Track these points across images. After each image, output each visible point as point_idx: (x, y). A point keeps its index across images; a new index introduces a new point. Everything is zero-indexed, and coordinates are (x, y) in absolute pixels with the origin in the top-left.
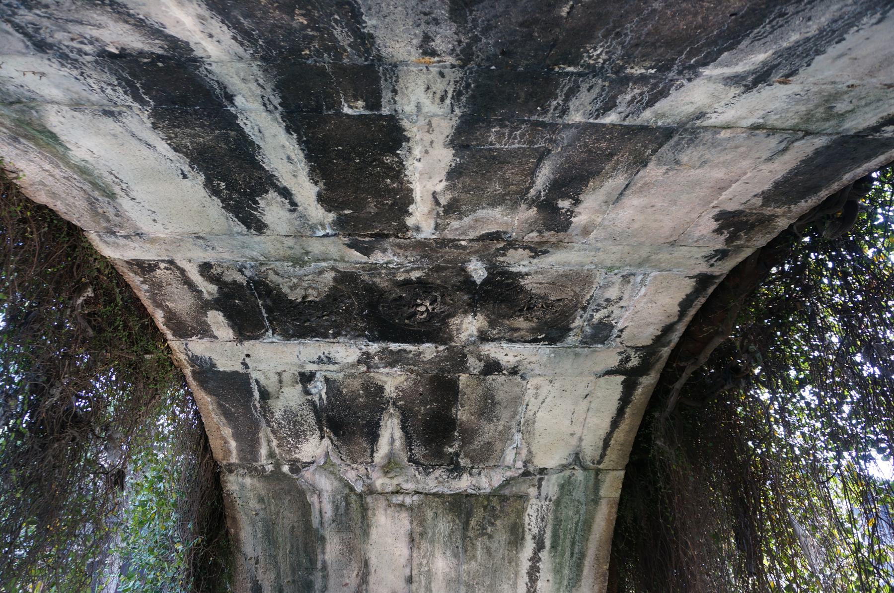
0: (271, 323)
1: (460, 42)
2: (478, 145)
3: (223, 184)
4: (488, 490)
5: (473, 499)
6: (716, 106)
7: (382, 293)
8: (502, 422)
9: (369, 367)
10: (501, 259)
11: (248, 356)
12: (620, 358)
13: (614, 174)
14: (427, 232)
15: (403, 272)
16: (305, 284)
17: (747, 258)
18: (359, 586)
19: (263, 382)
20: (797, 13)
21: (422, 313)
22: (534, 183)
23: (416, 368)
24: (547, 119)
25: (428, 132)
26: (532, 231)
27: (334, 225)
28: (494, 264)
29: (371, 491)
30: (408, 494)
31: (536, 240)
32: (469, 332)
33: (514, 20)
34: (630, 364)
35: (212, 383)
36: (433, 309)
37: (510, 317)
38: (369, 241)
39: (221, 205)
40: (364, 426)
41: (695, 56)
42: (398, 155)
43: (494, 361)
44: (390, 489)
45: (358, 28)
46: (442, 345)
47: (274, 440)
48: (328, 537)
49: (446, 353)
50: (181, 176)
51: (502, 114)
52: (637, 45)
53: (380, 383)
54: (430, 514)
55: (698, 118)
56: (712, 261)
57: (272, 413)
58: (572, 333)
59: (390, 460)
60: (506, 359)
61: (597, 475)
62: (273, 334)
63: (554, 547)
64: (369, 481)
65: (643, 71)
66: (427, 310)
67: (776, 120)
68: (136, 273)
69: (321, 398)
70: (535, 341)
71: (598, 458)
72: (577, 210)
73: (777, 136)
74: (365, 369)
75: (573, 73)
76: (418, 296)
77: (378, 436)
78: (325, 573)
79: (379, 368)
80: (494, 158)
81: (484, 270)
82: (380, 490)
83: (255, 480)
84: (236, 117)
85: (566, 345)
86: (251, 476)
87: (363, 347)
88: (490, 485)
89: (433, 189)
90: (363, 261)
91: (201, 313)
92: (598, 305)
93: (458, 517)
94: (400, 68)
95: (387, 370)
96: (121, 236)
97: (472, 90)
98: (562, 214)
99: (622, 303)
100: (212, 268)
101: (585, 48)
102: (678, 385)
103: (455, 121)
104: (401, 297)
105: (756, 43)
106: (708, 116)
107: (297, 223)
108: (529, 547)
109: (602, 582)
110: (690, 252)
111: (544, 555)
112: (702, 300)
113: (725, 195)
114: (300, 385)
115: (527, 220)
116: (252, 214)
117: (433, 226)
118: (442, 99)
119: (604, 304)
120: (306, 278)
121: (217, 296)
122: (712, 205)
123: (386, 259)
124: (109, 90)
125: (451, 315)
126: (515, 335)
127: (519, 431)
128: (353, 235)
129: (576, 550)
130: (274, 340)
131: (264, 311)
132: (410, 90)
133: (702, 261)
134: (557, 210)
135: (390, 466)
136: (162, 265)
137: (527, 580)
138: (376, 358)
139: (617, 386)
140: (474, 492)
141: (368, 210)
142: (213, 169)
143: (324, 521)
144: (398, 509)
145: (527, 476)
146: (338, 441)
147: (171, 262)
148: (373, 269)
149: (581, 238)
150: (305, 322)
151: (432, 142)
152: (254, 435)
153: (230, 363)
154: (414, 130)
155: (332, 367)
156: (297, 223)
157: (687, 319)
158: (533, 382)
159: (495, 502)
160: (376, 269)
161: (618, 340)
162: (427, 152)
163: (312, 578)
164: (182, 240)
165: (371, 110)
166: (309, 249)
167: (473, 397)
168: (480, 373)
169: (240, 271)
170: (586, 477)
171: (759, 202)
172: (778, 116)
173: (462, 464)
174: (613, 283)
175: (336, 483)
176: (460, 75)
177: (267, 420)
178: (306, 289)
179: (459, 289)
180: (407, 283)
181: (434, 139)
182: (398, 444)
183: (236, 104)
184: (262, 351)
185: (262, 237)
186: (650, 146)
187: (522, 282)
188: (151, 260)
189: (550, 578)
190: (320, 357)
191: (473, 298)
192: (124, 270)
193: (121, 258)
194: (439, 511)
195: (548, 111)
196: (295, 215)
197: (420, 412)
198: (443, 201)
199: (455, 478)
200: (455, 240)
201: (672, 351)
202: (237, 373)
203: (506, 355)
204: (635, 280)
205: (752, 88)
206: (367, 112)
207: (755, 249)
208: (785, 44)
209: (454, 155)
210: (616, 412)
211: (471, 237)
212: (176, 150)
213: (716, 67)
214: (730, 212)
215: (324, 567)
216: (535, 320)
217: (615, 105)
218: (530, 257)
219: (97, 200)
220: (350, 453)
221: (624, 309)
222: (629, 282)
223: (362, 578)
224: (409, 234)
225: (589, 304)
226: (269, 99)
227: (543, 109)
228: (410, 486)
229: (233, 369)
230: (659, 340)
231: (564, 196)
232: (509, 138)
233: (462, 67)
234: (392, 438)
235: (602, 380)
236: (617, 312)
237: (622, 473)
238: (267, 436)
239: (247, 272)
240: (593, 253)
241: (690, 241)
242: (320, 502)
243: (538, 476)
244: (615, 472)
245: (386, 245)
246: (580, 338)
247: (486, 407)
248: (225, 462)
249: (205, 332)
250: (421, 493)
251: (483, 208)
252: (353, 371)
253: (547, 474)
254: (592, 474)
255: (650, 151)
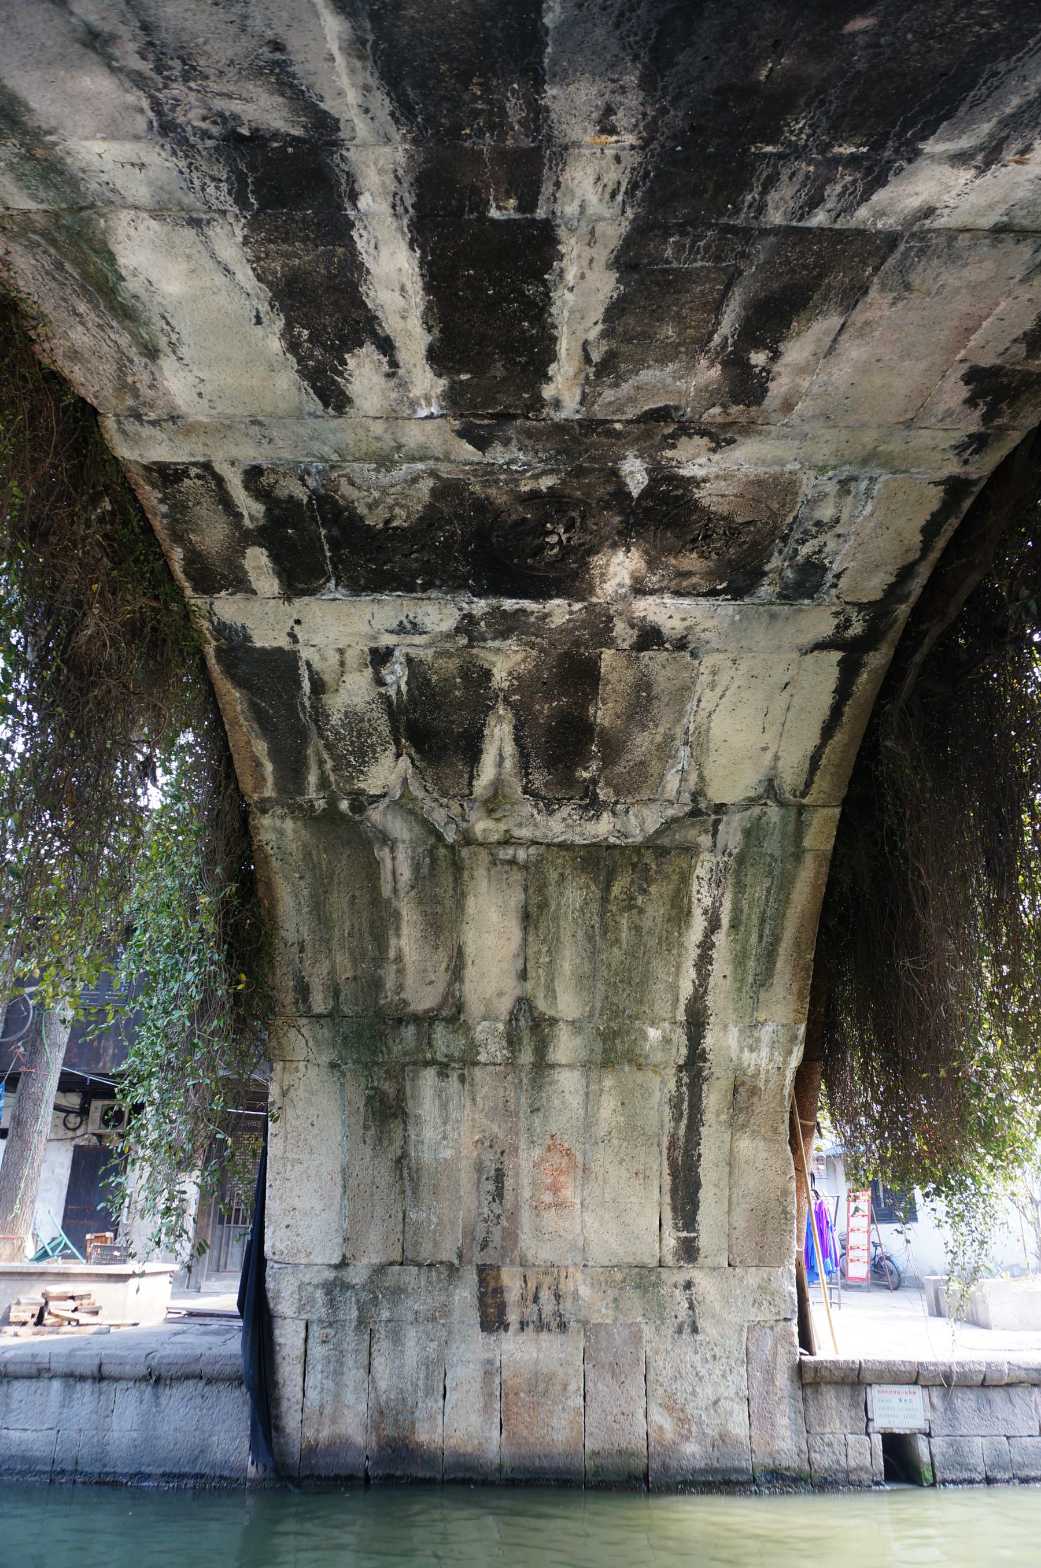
0: (335, 568)
1: (645, 115)
2: (650, 263)
3: (306, 332)
4: (639, 839)
5: (617, 852)
6: (946, 197)
7: (498, 513)
8: (661, 729)
9: (471, 639)
10: (668, 453)
11: (298, 622)
12: (836, 622)
13: (825, 308)
14: (570, 408)
15: (530, 478)
16: (390, 501)
17: (1017, 448)
18: (450, 984)
19: (317, 666)
20: (1010, 71)
21: (552, 548)
22: (719, 323)
23: (539, 640)
24: (739, 221)
25: (589, 244)
26: (714, 405)
27: (444, 399)
28: (659, 463)
29: (467, 839)
30: (522, 844)
31: (719, 420)
32: (617, 580)
33: (707, 87)
34: (851, 632)
35: (244, 667)
36: (569, 539)
37: (677, 552)
38: (488, 425)
39: (296, 367)
40: (461, 736)
41: (911, 127)
42: (544, 282)
43: (653, 628)
44: (495, 837)
45: (536, 100)
46: (578, 601)
47: (329, 761)
48: (404, 912)
49: (584, 615)
50: (254, 320)
51: (684, 216)
52: (844, 115)
53: (486, 666)
54: (553, 876)
55: (926, 217)
56: (966, 455)
57: (328, 716)
58: (766, 581)
59: (496, 790)
60: (670, 623)
61: (800, 814)
62: (337, 585)
63: (734, 926)
64: (465, 825)
65: (853, 150)
66: (560, 541)
67: (1024, 217)
68: (154, 486)
69: (399, 691)
70: (713, 593)
71: (802, 788)
72: (776, 368)
73: (1029, 241)
74: (465, 641)
75: (772, 154)
76: (548, 518)
77: (480, 752)
78: (400, 966)
79: (485, 640)
80: (669, 283)
81: (644, 473)
82: (480, 839)
83: (299, 823)
84: (353, 225)
85: (757, 601)
86: (293, 818)
87: (465, 605)
88: (642, 830)
89: (584, 337)
90: (476, 459)
91: (237, 551)
92: (806, 532)
93: (595, 880)
94: (571, 151)
95: (497, 644)
96: (149, 422)
97: (651, 181)
98: (756, 376)
99: (839, 529)
100: (262, 475)
101: (785, 119)
102: (918, 658)
103: (625, 227)
104: (524, 519)
105: (975, 109)
106: (938, 212)
107: (394, 395)
108: (699, 924)
109: (804, 979)
110: (934, 439)
111: (721, 938)
112: (954, 522)
113: (976, 339)
114: (370, 670)
115: (707, 387)
116: (334, 382)
117: (578, 398)
118: (613, 195)
119: (814, 529)
120: (392, 490)
121: (262, 522)
122: (959, 357)
123: (507, 457)
124: (211, 189)
125: (593, 550)
126: (685, 584)
127: (686, 743)
128: (467, 416)
129: (767, 932)
130: (338, 596)
131: (326, 547)
132: (576, 181)
133: (951, 454)
134: (746, 367)
135: (493, 803)
136: (194, 471)
137: (694, 976)
138: (483, 623)
139: (830, 669)
140: (618, 842)
141: (492, 373)
142: (298, 308)
143: (398, 887)
144: (507, 868)
145: (696, 816)
146: (422, 760)
147: (207, 466)
148: (488, 473)
149: (780, 416)
150: (385, 564)
151: (591, 261)
152: (300, 752)
153: (271, 634)
154: (571, 246)
155: (418, 639)
156: (394, 395)
157: (934, 555)
158: (709, 660)
159: (649, 858)
160: (492, 473)
161: (833, 591)
162: (583, 277)
163: (381, 972)
164: (230, 427)
165: (524, 212)
166: (403, 441)
167: (620, 687)
168: (632, 647)
169: (302, 479)
170: (783, 818)
171: (1021, 350)
172: (1025, 212)
173: (602, 797)
174: (826, 495)
175: (417, 828)
176: (639, 160)
177: (319, 728)
178: (391, 508)
179: (607, 507)
180: (534, 495)
181: (596, 256)
182: (508, 764)
183: (359, 205)
184: (319, 613)
185: (341, 421)
186: (870, 261)
187: (698, 494)
188: (178, 464)
189: (728, 973)
190: (401, 622)
191: (625, 521)
192: (137, 477)
193: (139, 459)
194: (567, 872)
195: (741, 209)
196: (393, 383)
197: (541, 713)
198: (596, 357)
199: (590, 819)
200: (606, 422)
201: (913, 610)
202: (280, 650)
203: (671, 617)
204: (857, 488)
205: (984, 171)
206: (517, 216)
207: (1025, 432)
208: (1008, 111)
209: (618, 281)
210: (828, 713)
211: (630, 417)
212: (259, 278)
213: (937, 142)
214: (983, 369)
215: (399, 958)
216: (714, 556)
217: (822, 200)
218: (710, 450)
219: (131, 361)
220: (438, 781)
221: (842, 539)
222: (849, 492)
223: (454, 973)
224: (545, 411)
225: (791, 530)
226: (401, 199)
227: (734, 207)
228: (525, 833)
229: (275, 644)
230: (894, 592)
231: (759, 345)
232: (690, 252)
233: (642, 148)
234: (500, 755)
235: (809, 657)
236: (832, 545)
237: (837, 811)
238: (318, 754)
239: (311, 482)
240: (797, 443)
241: (933, 420)
242: (394, 859)
243: (713, 817)
244: (826, 810)
245: (511, 433)
246: (778, 589)
247: (638, 704)
248: (256, 797)
249: (240, 584)
250: (541, 844)
251: (649, 367)
252: (448, 645)
253: (725, 813)
254: (793, 813)
255: (870, 269)
